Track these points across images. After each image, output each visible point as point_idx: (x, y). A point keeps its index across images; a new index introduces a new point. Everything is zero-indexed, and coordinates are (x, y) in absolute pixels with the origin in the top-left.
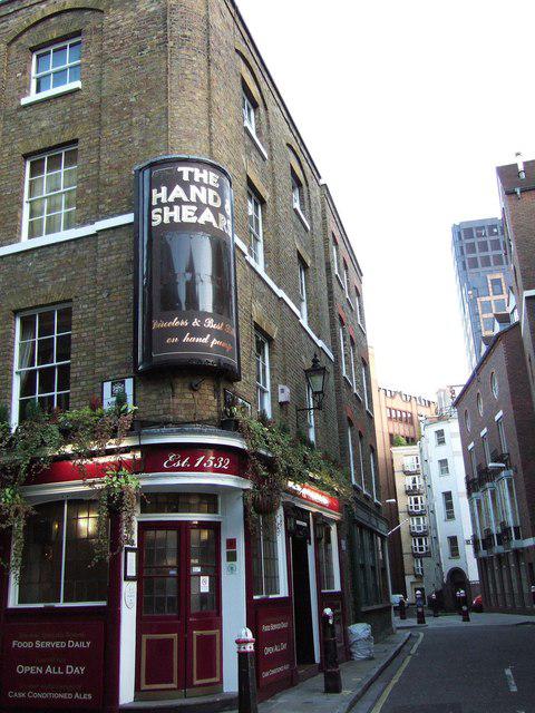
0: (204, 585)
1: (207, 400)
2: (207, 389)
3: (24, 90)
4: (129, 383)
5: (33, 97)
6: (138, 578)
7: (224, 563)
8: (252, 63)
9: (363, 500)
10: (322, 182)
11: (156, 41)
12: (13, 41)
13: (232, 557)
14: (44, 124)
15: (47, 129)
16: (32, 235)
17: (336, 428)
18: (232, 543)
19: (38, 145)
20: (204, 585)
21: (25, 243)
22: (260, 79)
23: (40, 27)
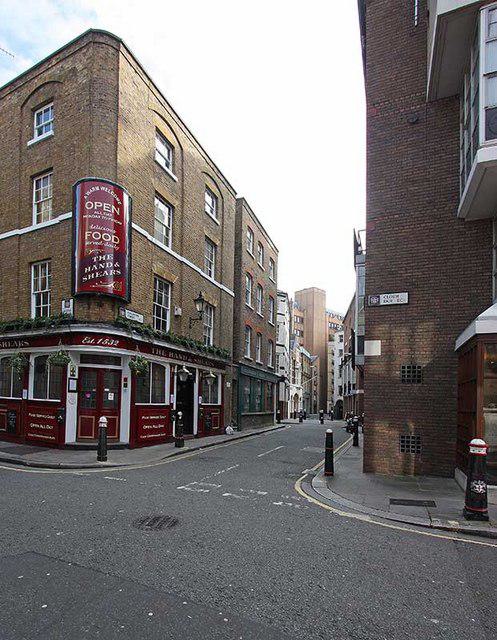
0: (111, 397)
1: (108, 313)
2: (107, 307)
3: (32, 136)
4: (71, 301)
5: (37, 139)
6: (78, 390)
7: (123, 388)
8: (168, 118)
9: (329, 361)
10: (237, 197)
11: (86, 103)
12: (24, 103)
13: (126, 386)
14: (38, 158)
15: (39, 160)
16: (38, 222)
17: (232, 330)
18: (126, 379)
19: (36, 171)
20: (111, 397)
21: (35, 226)
22: (175, 126)
23: (35, 95)
